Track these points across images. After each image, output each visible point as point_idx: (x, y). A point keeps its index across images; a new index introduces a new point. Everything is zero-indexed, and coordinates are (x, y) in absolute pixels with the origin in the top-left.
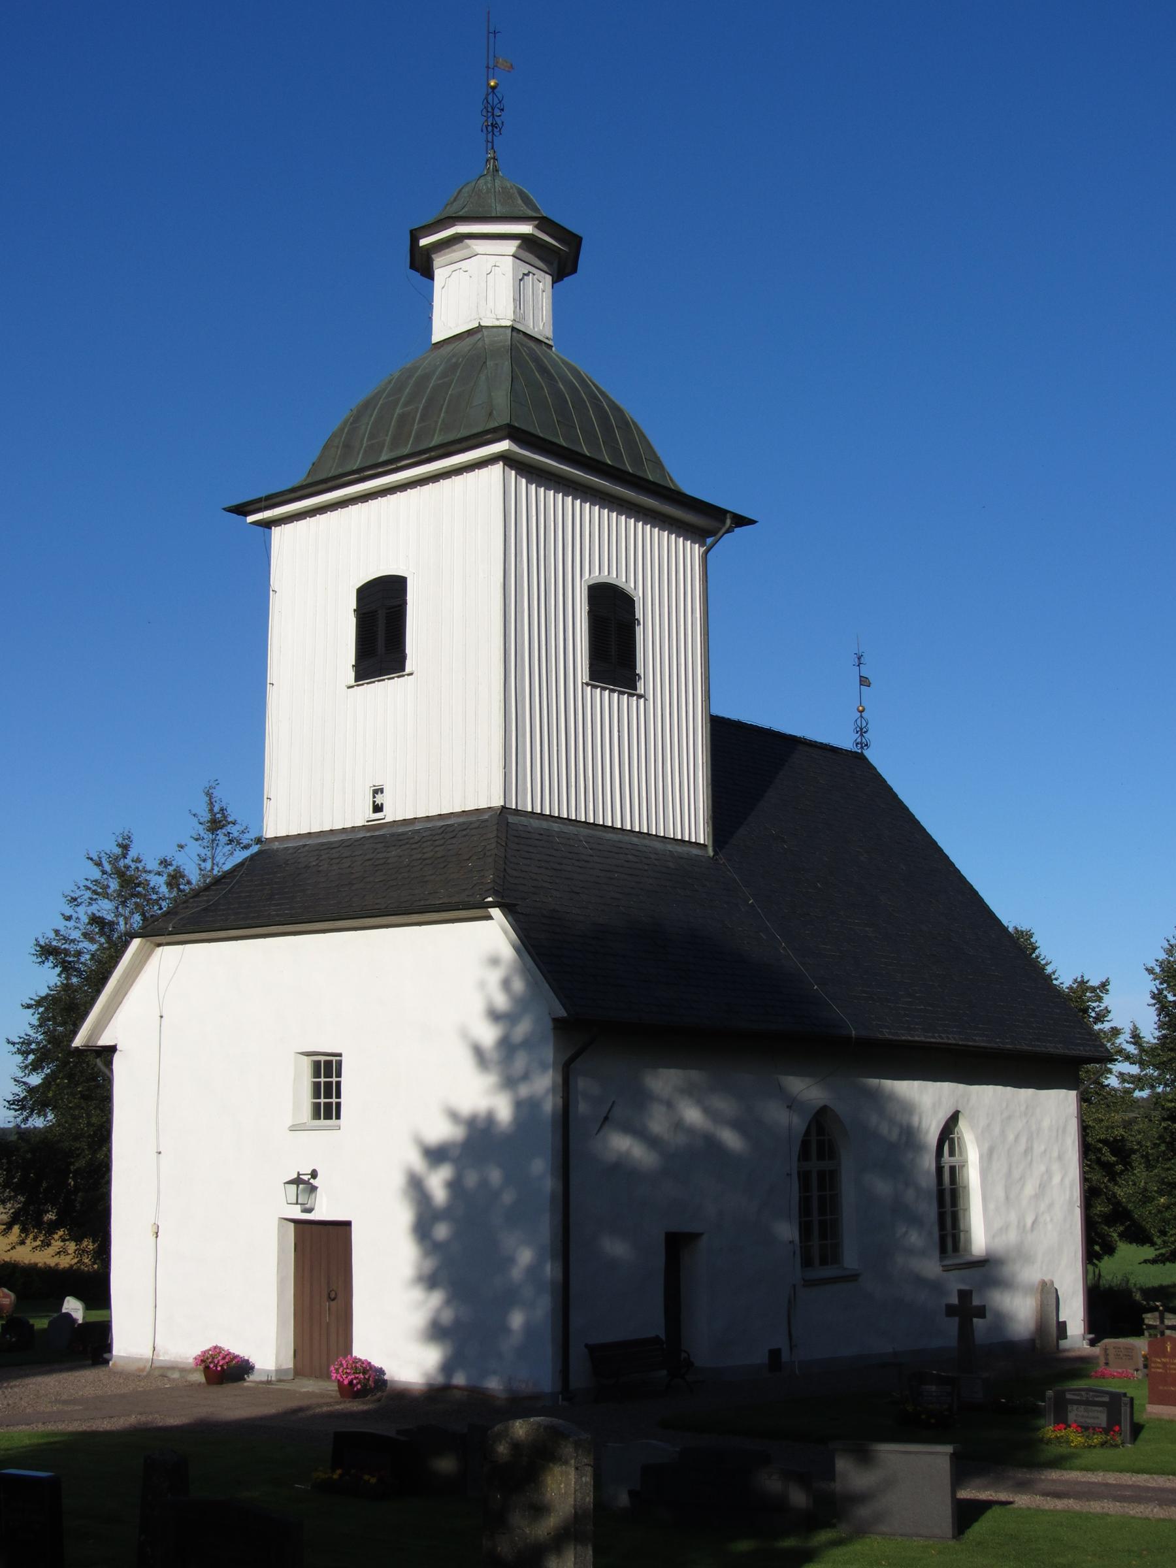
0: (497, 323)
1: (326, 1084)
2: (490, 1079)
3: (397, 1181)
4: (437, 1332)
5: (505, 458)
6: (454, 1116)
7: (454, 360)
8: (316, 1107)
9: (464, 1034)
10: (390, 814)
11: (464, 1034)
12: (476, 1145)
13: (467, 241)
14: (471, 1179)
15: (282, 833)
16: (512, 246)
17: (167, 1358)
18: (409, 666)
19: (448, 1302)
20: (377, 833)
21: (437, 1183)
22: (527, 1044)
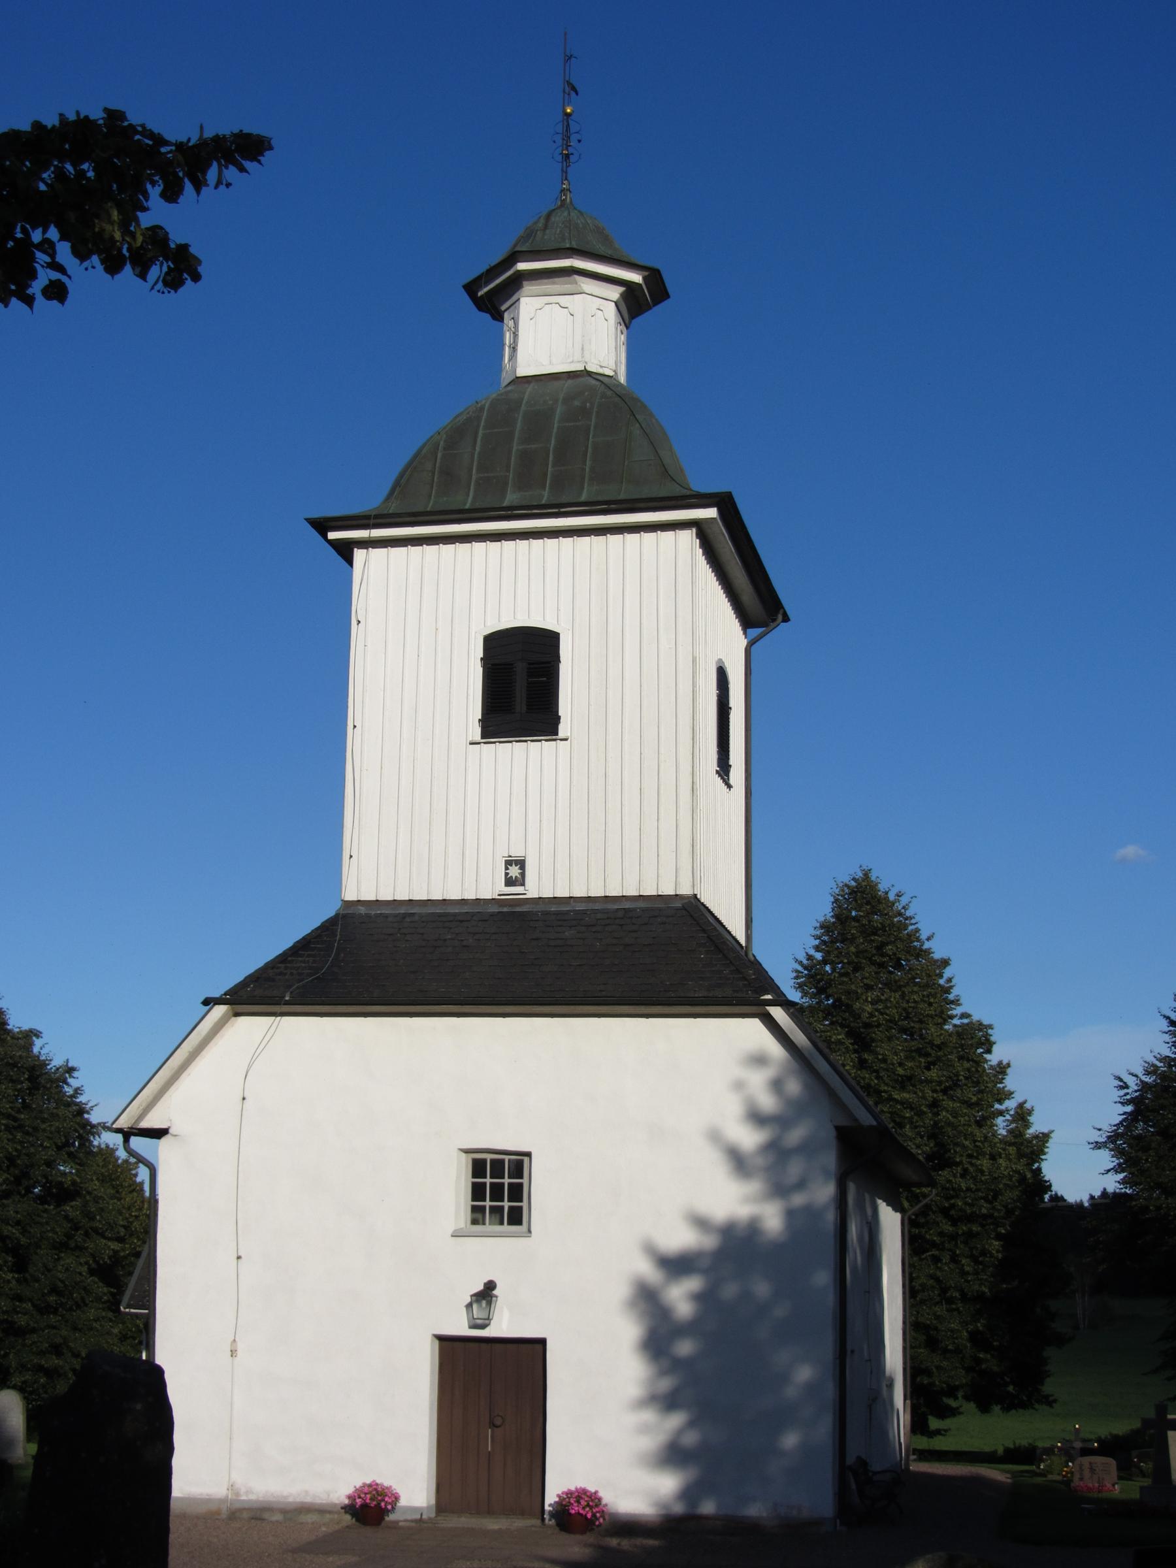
0: (601, 371)
1: (498, 1188)
2: (754, 1186)
3: (620, 1291)
4: (673, 1455)
5: (697, 525)
6: (701, 1223)
7: (577, 403)
8: (475, 1209)
9: (714, 1136)
10: (537, 886)
11: (714, 1136)
12: (732, 1253)
13: (577, 277)
14: (730, 1291)
15: (368, 895)
16: (615, 293)
17: (252, 1497)
18: (563, 730)
19: (691, 1424)
20: (518, 909)
21: (681, 1297)
22: (806, 1149)
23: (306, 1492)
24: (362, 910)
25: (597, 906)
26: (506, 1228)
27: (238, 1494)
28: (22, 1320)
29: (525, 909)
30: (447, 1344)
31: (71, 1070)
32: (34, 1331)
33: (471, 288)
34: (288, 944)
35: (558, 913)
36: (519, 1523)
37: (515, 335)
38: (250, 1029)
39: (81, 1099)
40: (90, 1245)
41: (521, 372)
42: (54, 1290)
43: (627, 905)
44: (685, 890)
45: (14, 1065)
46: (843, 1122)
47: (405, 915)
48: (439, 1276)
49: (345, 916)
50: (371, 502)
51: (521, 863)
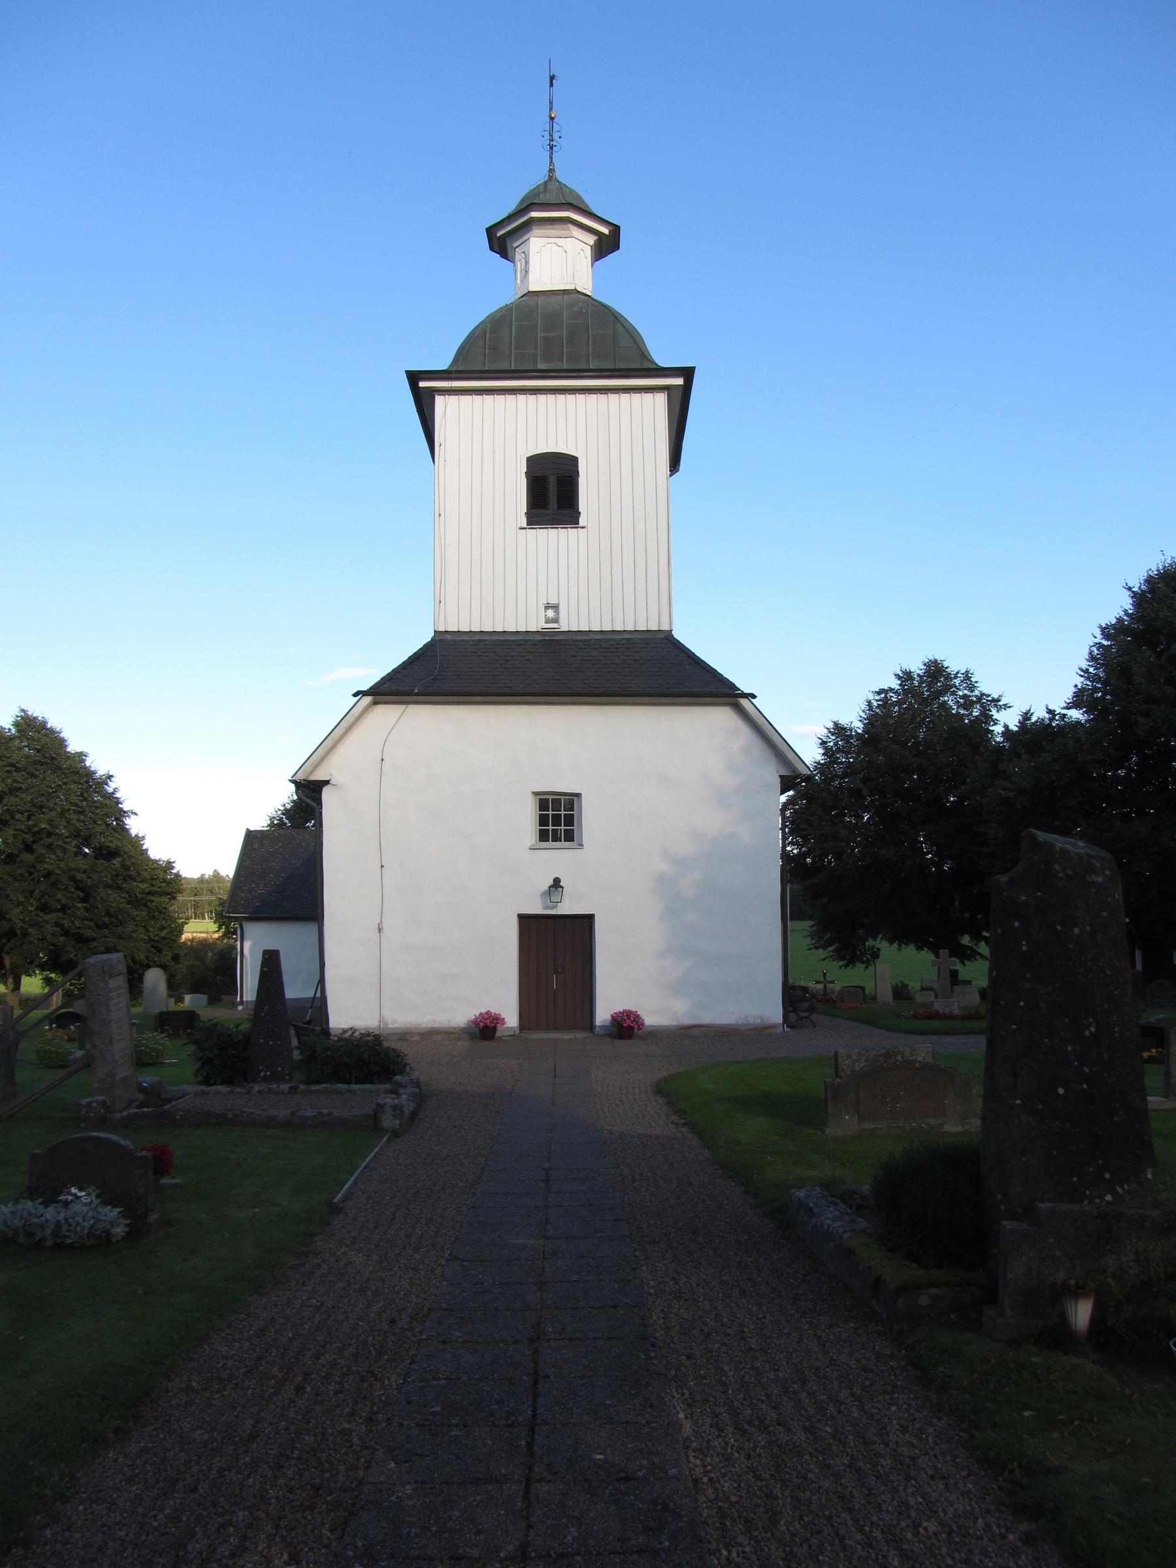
1: (557, 818)
7: (576, 309)
13: (570, 226)
16: (591, 239)
24: (449, 637)
25: (608, 637)
26: (563, 844)
27: (387, 1024)
28: (88, 933)
29: (561, 637)
30: (526, 921)
31: (110, 777)
32: (94, 939)
33: (490, 231)
34: (404, 657)
36: (580, 1035)
37: (527, 263)
38: (387, 714)
40: (126, 886)
42: (108, 914)
44: (665, 627)
45: (77, 773)
46: (785, 773)
48: (527, 875)
49: (440, 641)
51: (556, 607)
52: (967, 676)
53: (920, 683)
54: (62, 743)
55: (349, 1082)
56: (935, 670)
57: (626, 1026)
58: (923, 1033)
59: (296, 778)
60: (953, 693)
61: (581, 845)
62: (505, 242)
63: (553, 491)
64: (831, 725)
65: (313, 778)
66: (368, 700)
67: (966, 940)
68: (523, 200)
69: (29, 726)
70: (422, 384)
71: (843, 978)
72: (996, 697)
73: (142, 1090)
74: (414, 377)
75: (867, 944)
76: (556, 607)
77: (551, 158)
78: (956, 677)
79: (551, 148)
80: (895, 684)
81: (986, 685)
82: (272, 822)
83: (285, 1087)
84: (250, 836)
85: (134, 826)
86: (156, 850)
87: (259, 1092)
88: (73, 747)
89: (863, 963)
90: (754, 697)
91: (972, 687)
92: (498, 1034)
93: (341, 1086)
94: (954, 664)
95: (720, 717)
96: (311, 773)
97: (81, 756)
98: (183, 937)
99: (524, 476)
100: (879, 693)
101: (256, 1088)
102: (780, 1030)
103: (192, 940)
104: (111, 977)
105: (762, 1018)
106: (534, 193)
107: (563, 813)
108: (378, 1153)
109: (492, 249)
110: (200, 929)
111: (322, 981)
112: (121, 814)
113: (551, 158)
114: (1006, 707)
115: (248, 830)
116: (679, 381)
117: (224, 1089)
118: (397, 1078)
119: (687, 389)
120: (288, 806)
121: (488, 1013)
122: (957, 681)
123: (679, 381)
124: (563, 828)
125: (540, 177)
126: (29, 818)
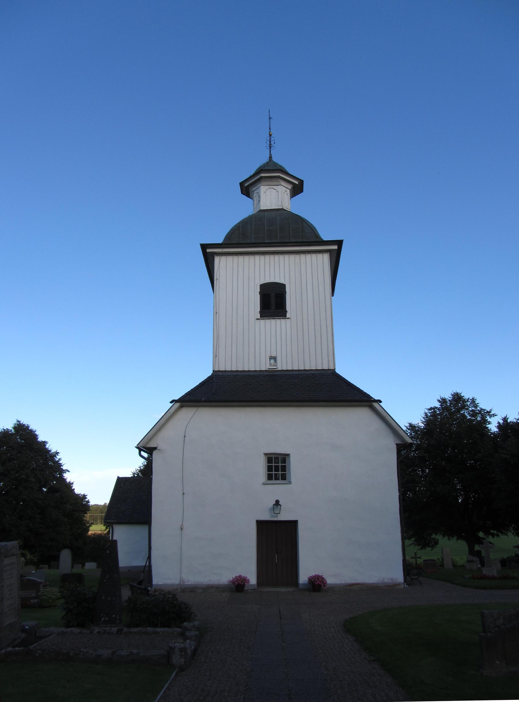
1: (277, 467)
13: (280, 180)
16: (290, 187)
17: (189, 583)
18: (288, 315)
23: (210, 580)
24: (220, 373)
25: (302, 373)
29: (278, 373)
30: (260, 524)
31: (57, 453)
34: (197, 383)
35: (290, 375)
36: (290, 589)
37: (259, 197)
38: (187, 413)
39: (61, 462)
41: (262, 208)
43: (312, 372)
46: (399, 442)
47: (236, 375)
48: (261, 499)
50: (220, 241)
51: (275, 358)
52: (473, 400)
53: (451, 404)
54: (35, 436)
55: (156, 626)
56: (457, 398)
57: (317, 584)
58: (485, 588)
59: (139, 446)
60: (467, 409)
61: (290, 483)
62: (248, 189)
63: (273, 301)
64: (407, 425)
65: (148, 446)
66: (178, 405)
67: (481, 534)
68: (259, 168)
69: (22, 430)
70: (208, 250)
71: (426, 555)
72: (489, 410)
73: (23, 630)
74: (204, 247)
75: (432, 537)
76: (275, 358)
77: (270, 152)
78: (468, 401)
79: (270, 148)
80: (438, 405)
81: (483, 404)
82: (134, 476)
83: (114, 629)
84: (121, 482)
85: (68, 477)
86: (78, 490)
87: (98, 632)
88: (41, 439)
89: (430, 547)
90: (380, 401)
91: (476, 406)
92: (246, 588)
93: (150, 629)
94: (467, 395)
95: (360, 415)
96: (148, 443)
97: (44, 443)
98: (90, 532)
99: (258, 294)
100: (431, 409)
101: (97, 630)
102: (402, 586)
103: (94, 534)
104: (6, 557)
105: (392, 579)
106: (264, 165)
107: (280, 464)
108: (168, 688)
109: (242, 193)
110: (97, 529)
111: (149, 558)
112: (62, 471)
113: (270, 152)
114: (494, 415)
115: (118, 477)
116: (335, 247)
117: (76, 630)
118: (185, 624)
119: (338, 252)
120: (142, 468)
121: (240, 576)
122: (468, 403)
123: (335, 247)
124: (280, 473)
125: (266, 159)
126: (16, 473)
